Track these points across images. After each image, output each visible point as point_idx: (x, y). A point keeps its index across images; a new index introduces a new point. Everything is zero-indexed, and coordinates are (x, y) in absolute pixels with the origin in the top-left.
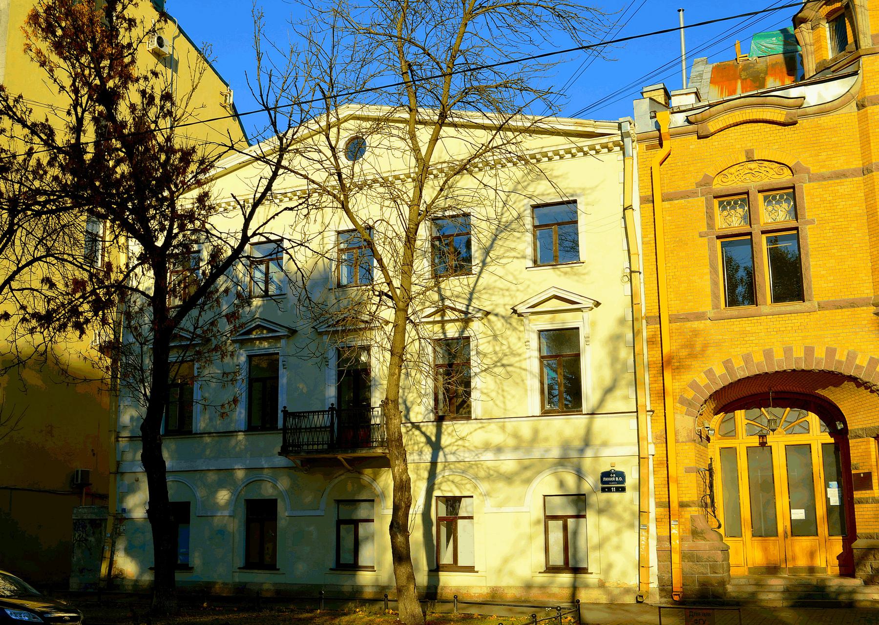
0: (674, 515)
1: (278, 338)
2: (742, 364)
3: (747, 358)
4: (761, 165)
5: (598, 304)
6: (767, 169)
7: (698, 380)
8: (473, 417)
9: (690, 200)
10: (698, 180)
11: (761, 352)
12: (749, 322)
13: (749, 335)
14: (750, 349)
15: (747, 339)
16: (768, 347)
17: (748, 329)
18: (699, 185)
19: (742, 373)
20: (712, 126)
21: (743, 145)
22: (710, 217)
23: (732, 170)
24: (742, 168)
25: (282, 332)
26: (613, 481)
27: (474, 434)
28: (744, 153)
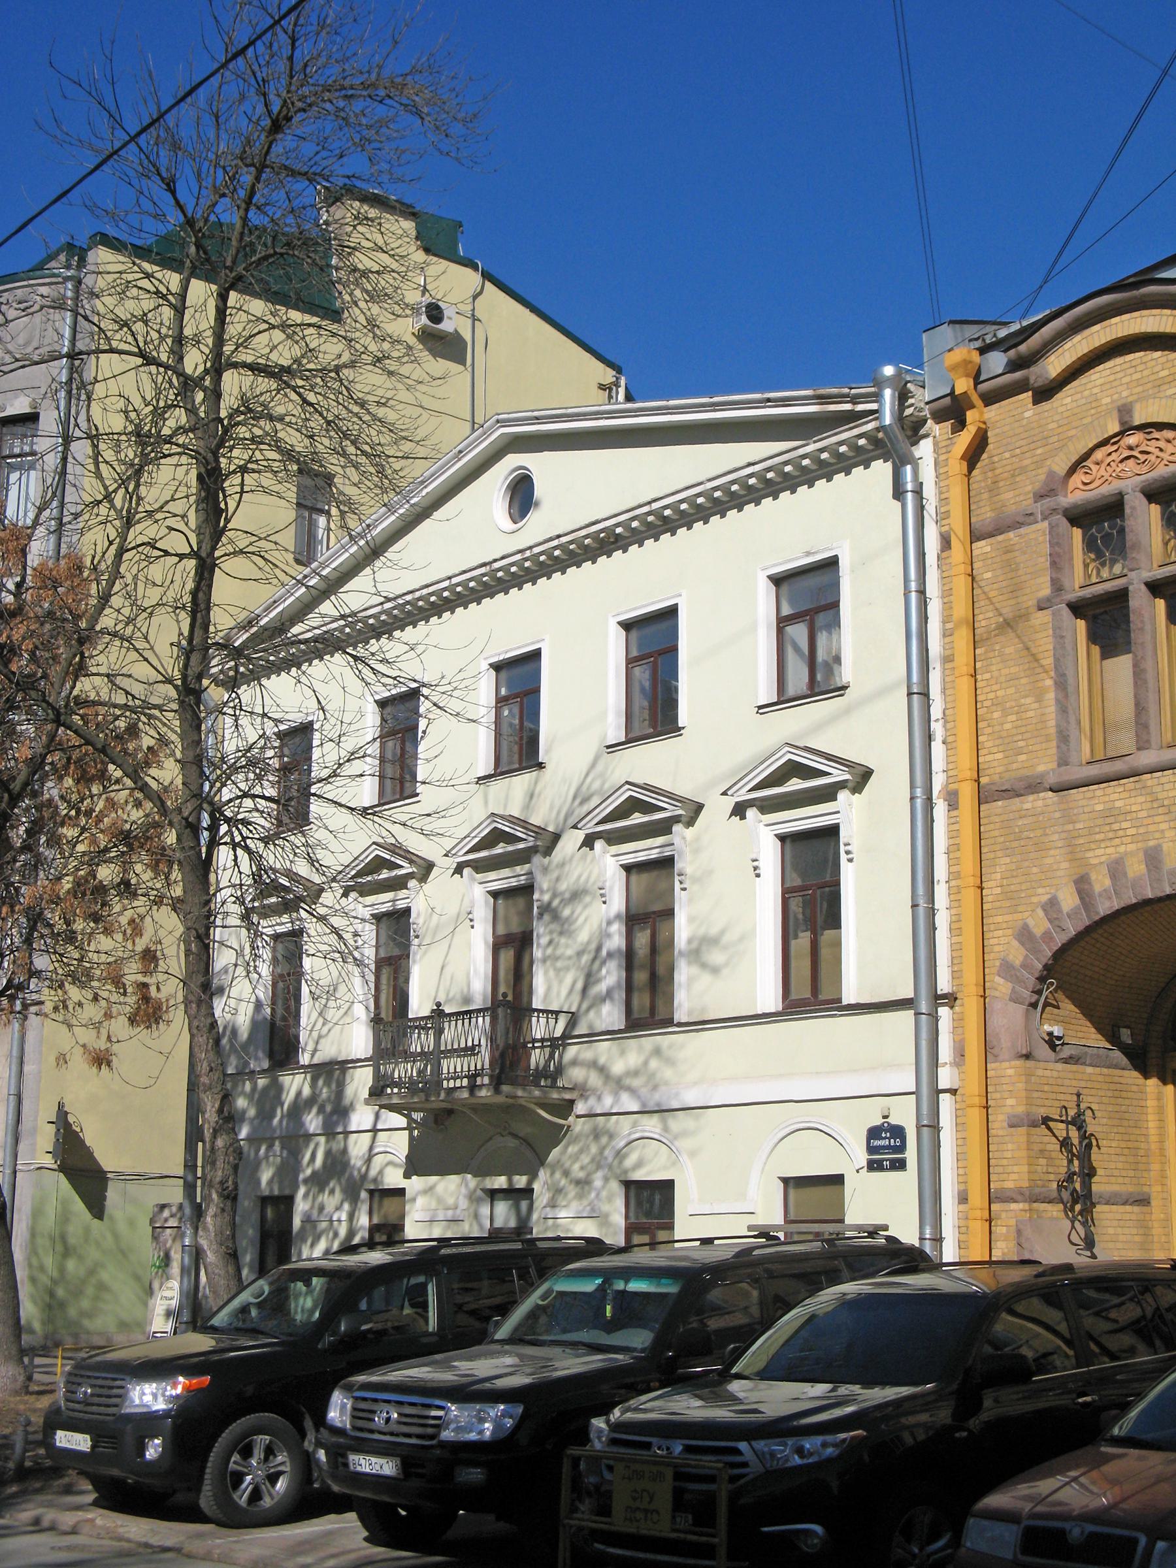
0: (390, 1137)
1: (828, 794)
2: (1107, 882)
3: (1116, 869)
4: (1149, 437)
5: (446, 855)
6: (1162, 444)
7: (1031, 923)
8: (680, 1016)
9: (1022, 531)
10: (1037, 486)
11: (1141, 855)
12: (1121, 789)
13: (1121, 818)
14: (1122, 849)
15: (1116, 826)
16: (1151, 843)
17: (1118, 804)
18: (1040, 496)
19: (1107, 904)
20: (1055, 364)
21: (1116, 397)
22: (1057, 562)
23: (1099, 454)
24: (1115, 447)
25: (838, 774)
26: (884, 1147)
27: (319, 1047)
28: (1115, 414)
